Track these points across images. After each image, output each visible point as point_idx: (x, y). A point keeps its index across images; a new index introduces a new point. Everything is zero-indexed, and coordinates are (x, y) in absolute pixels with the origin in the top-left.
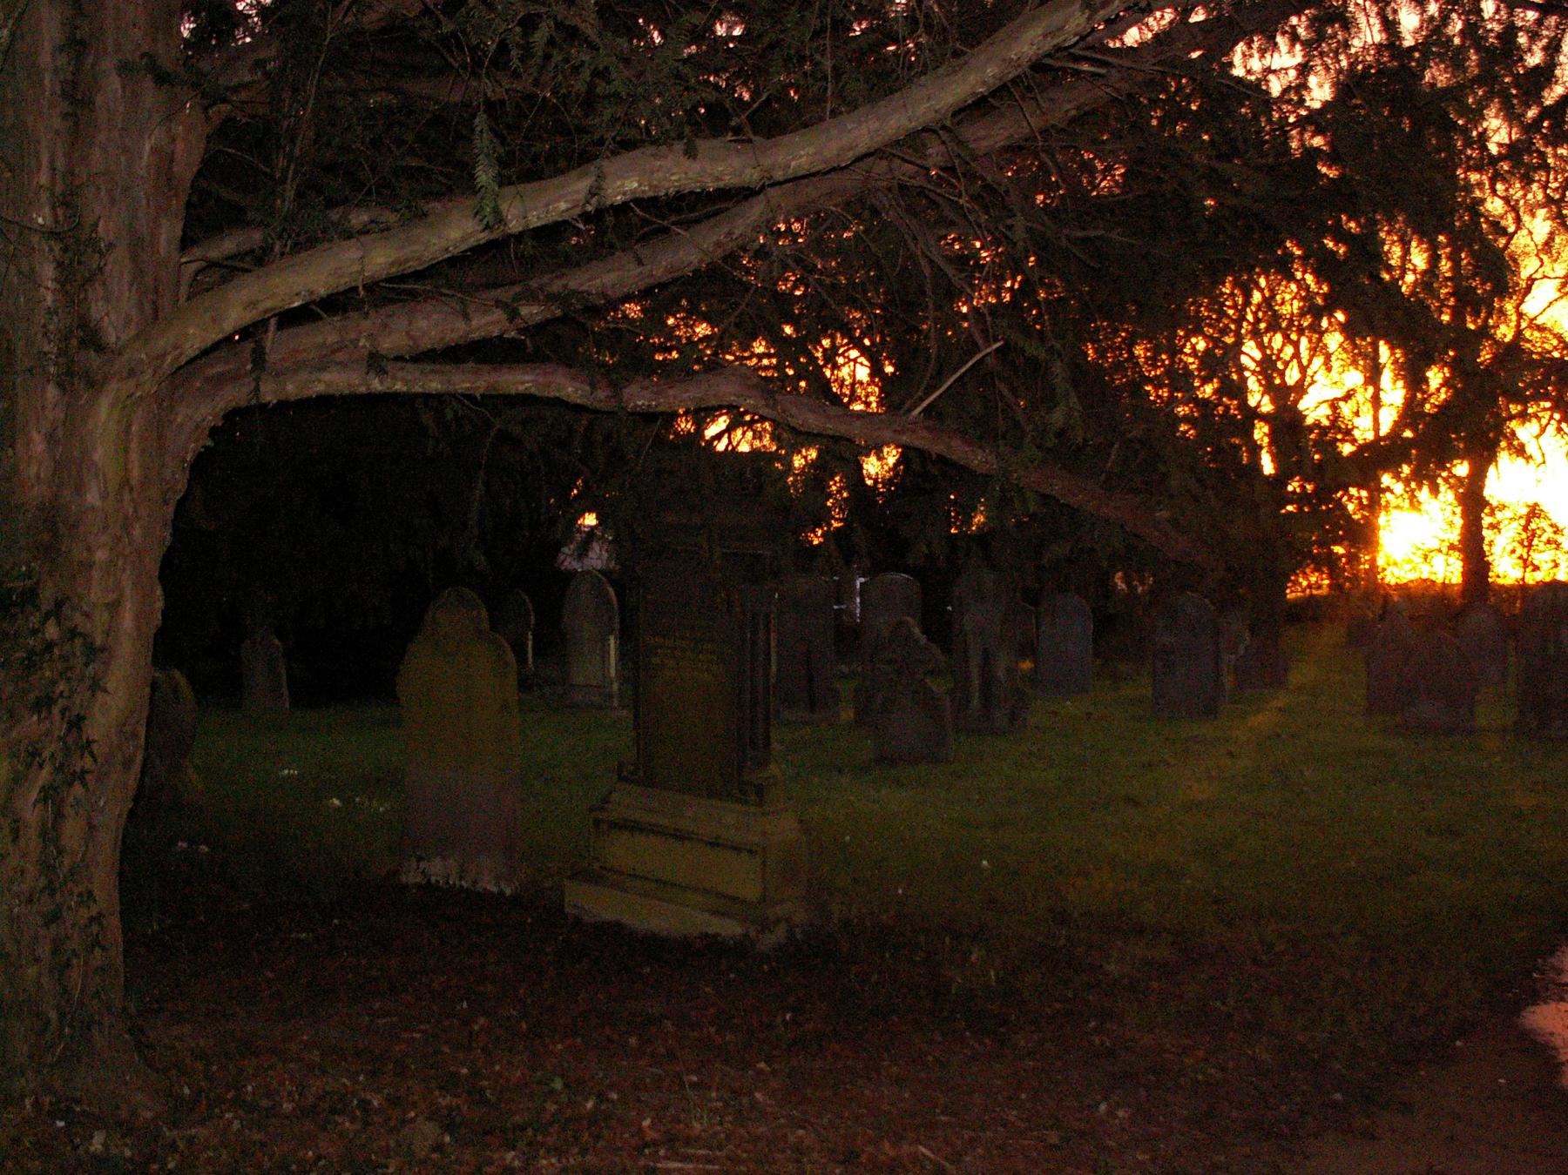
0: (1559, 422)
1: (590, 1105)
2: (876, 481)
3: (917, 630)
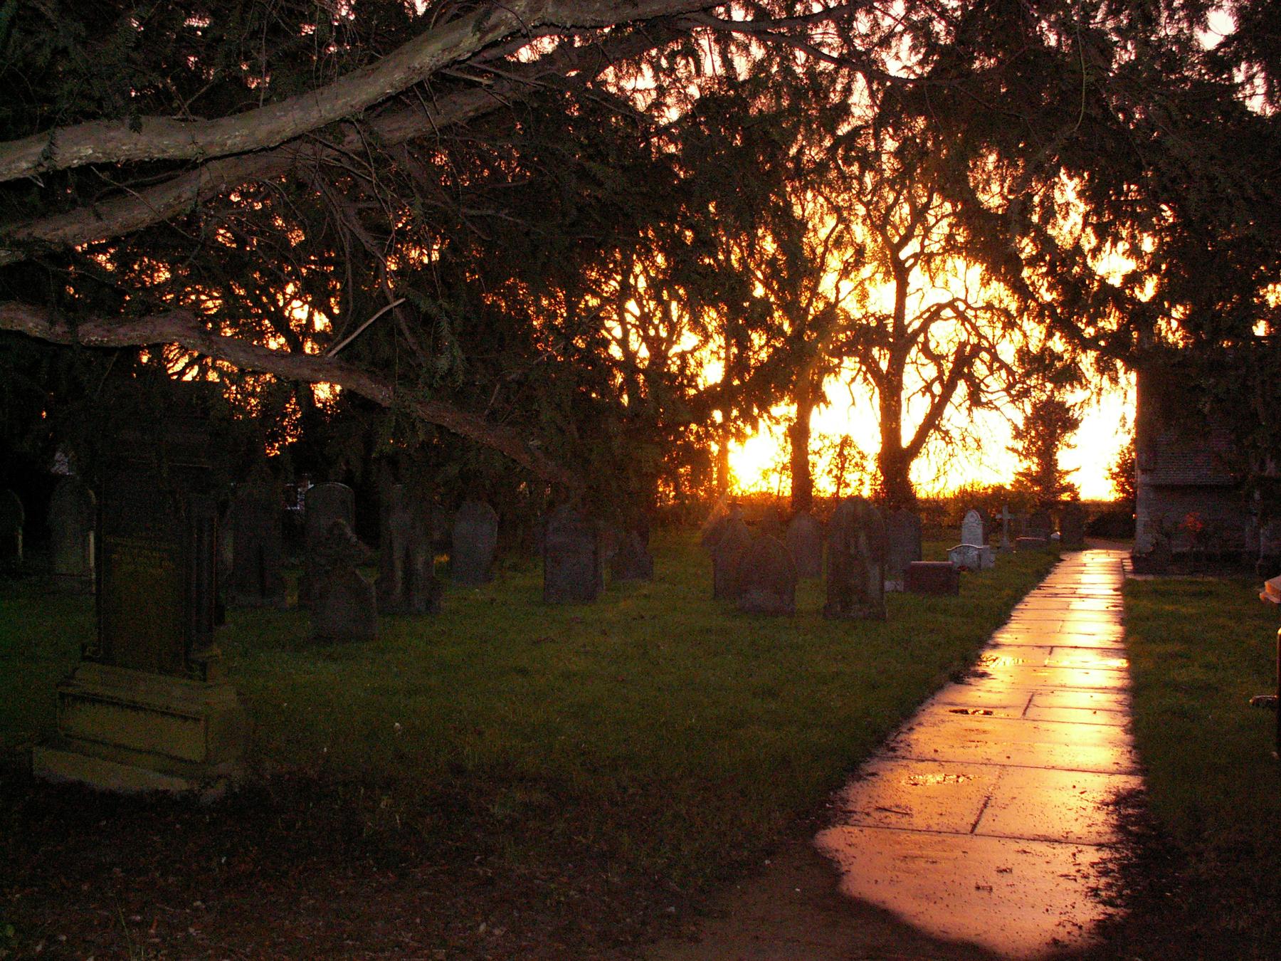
0: (865, 373)
1: (39, 948)
2: (325, 404)
3: (349, 532)
